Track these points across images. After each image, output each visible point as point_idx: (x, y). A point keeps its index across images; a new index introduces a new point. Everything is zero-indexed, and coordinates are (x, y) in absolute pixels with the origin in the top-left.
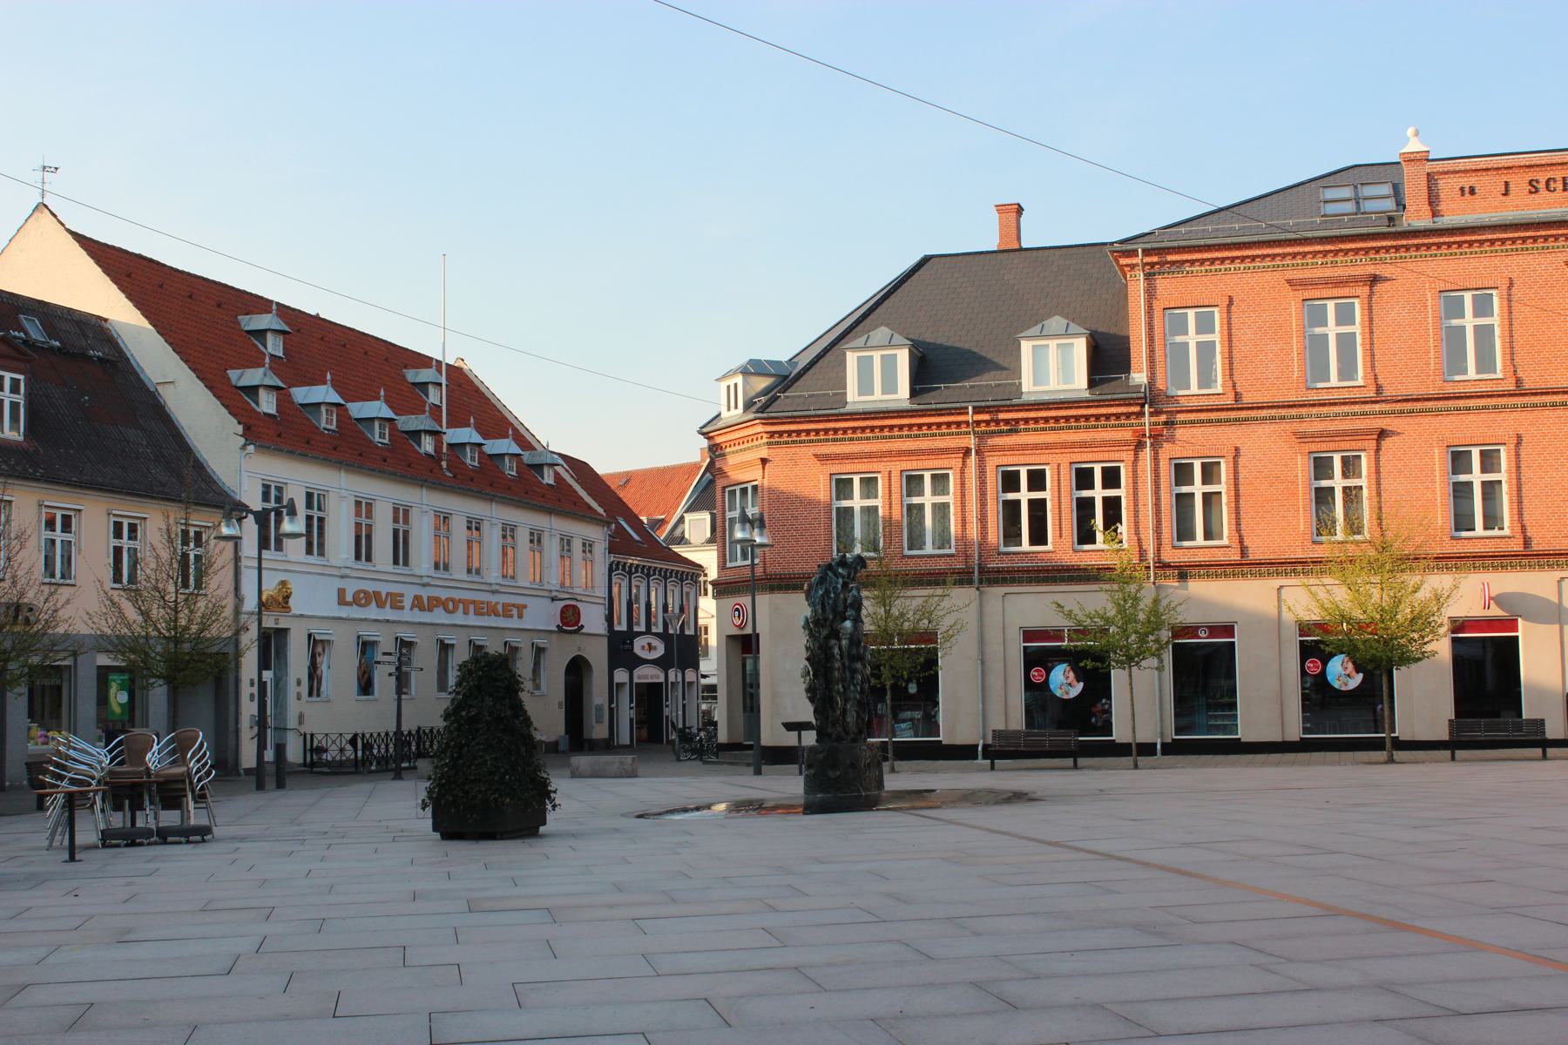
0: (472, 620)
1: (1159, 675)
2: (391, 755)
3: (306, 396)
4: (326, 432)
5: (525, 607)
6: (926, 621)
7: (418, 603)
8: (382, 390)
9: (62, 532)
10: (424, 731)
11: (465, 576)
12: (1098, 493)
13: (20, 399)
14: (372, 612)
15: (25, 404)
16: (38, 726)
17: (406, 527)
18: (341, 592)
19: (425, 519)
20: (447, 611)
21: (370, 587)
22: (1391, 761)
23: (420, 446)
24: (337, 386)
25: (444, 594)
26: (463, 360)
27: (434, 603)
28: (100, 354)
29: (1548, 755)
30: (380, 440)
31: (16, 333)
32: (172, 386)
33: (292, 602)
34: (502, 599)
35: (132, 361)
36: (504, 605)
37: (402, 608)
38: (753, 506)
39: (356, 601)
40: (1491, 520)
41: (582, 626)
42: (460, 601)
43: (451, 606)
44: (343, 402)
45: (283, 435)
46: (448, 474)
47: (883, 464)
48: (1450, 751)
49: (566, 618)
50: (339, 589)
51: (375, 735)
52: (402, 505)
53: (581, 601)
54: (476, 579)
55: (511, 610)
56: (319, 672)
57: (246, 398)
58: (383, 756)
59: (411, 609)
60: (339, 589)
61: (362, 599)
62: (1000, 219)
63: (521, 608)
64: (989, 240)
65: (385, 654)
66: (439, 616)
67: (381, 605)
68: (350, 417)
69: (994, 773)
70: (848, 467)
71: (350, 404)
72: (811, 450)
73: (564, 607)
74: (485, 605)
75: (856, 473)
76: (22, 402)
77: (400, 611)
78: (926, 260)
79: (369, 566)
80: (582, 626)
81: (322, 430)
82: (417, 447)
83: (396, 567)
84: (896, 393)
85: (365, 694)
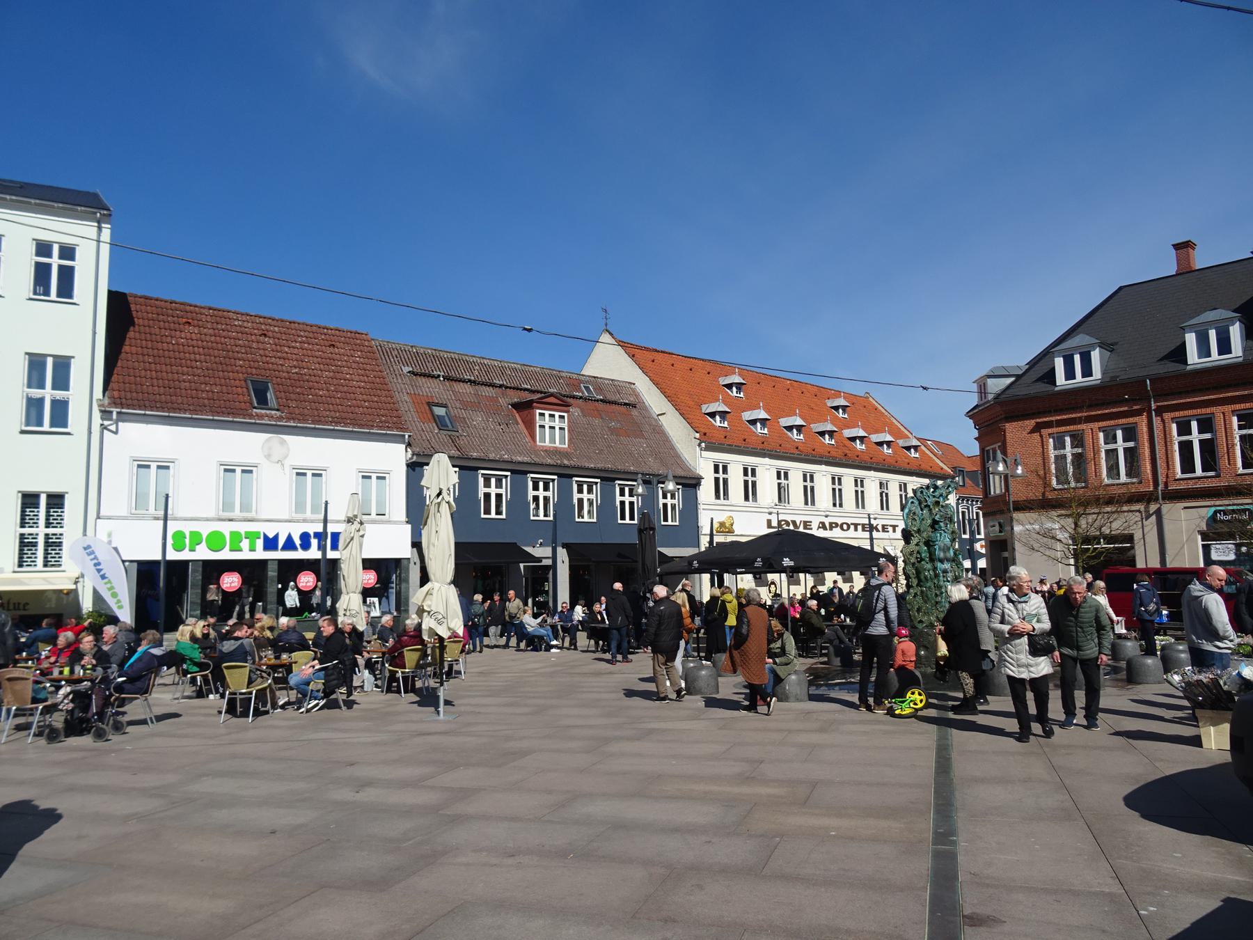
3: (749, 416)
5: (897, 526)
12: (1195, 437)
13: (565, 425)
16: (81, 643)
17: (812, 484)
20: (842, 529)
24: (767, 411)
25: (840, 521)
28: (601, 397)
40: (1133, 470)
42: (852, 524)
43: (845, 527)
62: (1177, 253)
64: (1169, 267)
68: (780, 427)
71: (872, 436)
78: (1121, 288)
79: (726, 502)
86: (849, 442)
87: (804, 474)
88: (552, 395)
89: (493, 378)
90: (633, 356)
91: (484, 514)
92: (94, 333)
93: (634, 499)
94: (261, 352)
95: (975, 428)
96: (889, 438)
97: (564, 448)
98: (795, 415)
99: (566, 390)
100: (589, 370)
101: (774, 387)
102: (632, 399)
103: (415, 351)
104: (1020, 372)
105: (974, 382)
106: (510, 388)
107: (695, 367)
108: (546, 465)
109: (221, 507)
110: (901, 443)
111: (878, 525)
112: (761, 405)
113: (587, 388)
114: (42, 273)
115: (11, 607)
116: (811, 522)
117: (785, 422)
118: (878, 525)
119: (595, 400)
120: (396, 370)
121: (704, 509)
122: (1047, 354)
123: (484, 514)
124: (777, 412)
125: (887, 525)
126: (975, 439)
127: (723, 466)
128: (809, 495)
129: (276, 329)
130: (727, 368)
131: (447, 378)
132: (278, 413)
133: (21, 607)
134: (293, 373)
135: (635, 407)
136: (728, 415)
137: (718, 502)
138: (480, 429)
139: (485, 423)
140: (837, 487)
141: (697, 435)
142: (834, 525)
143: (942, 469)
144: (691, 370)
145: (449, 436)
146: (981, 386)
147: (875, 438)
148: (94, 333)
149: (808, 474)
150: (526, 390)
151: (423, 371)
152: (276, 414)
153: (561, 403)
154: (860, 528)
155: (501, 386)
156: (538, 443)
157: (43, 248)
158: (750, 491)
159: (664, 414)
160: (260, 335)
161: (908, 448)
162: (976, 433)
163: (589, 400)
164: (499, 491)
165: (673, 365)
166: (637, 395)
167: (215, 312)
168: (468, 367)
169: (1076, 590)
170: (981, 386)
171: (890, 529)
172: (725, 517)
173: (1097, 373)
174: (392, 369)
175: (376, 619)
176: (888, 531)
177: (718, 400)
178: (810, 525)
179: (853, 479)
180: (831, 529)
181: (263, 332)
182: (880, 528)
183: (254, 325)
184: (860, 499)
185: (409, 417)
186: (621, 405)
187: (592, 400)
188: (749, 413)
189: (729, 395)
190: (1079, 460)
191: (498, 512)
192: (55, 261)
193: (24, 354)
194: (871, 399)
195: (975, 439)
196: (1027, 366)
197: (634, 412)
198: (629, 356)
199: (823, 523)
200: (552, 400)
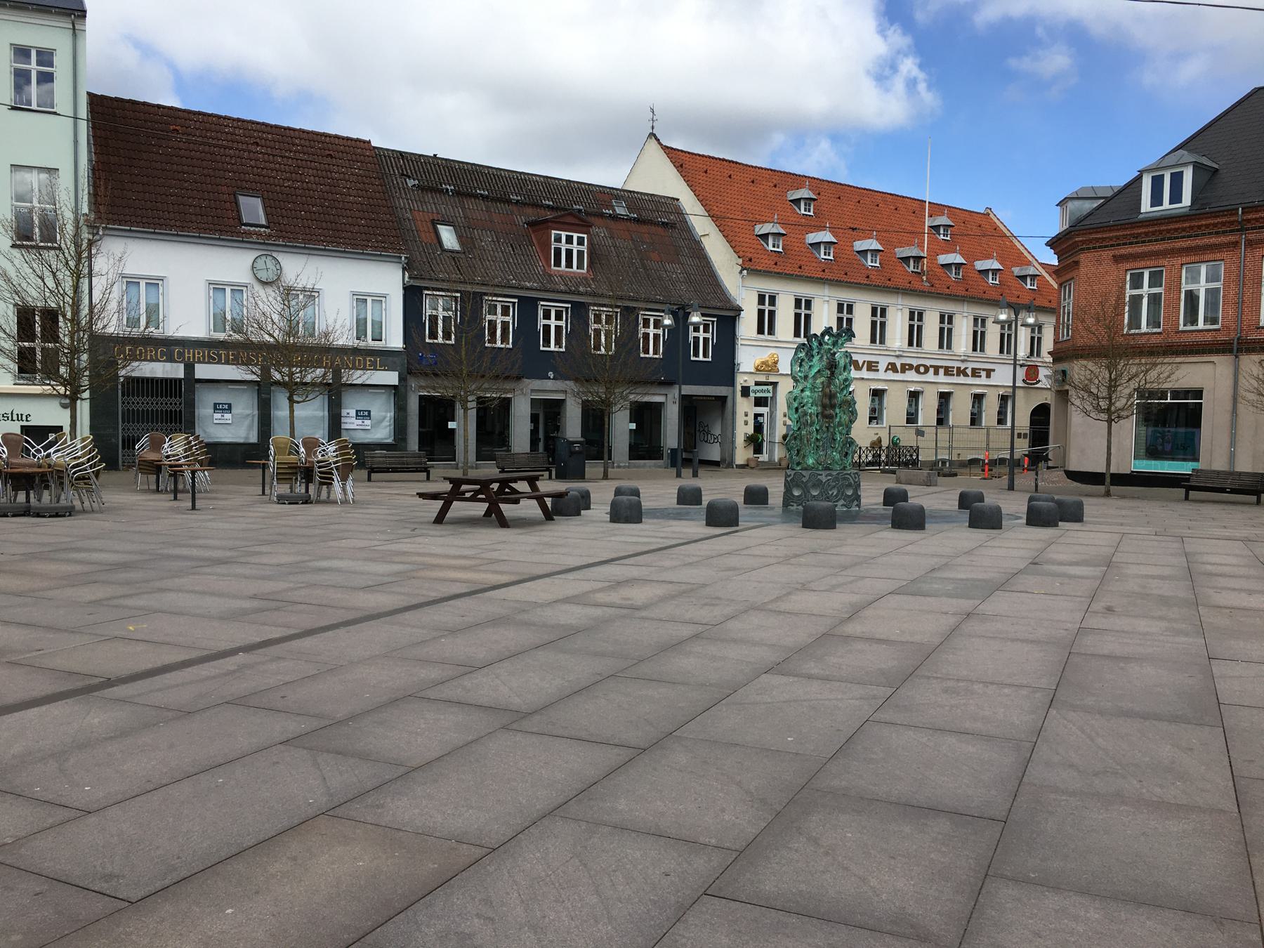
0: (942, 378)
2: (863, 462)
3: (861, 246)
5: (994, 370)
7: (892, 367)
9: (556, 320)
13: (584, 248)
20: (918, 371)
22: (1108, 494)
24: (833, 230)
25: (915, 363)
27: (905, 368)
28: (635, 215)
29: (1190, 497)
33: (779, 366)
36: (974, 370)
37: (878, 370)
42: (931, 366)
43: (922, 369)
48: (1256, 497)
51: (864, 449)
55: (980, 373)
58: (856, 462)
59: (886, 371)
69: (1187, 503)
72: (1107, 254)
74: (955, 370)
75: (1204, 262)
76: (586, 251)
77: (876, 372)
79: (770, 337)
81: (820, 259)
86: (859, 257)
91: (543, 346)
92: (76, 142)
93: (660, 332)
94: (252, 163)
97: (583, 273)
98: (955, 252)
103: (422, 161)
104: (1110, 194)
105: (1057, 205)
106: (529, 205)
109: (212, 327)
114: (21, 78)
115: (15, 417)
116: (878, 363)
120: (400, 184)
121: (741, 345)
123: (543, 346)
124: (971, 257)
125: (980, 369)
127: (948, 316)
129: (270, 136)
131: (457, 193)
132: (268, 231)
133: (24, 418)
134: (286, 187)
137: (761, 336)
138: (489, 251)
139: (495, 245)
140: (979, 329)
141: (740, 261)
142: (907, 367)
144: (753, 182)
145: (454, 258)
148: (76, 142)
151: (499, 196)
152: (265, 232)
153: (579, 222)
154: (941, 371)
156: (552, 267)
157: (22, 52)
159: (708, 235)
160: (252, 144)
164: (559, 323)
165: (730, 177)
167: (205, 118)
168: (482, 180)
169: (934, 459)
171: (983, 374)
172: (767, 356)
173: (1187, 199)
174: (395, 182)
175: (372, 446)
176: (980, 376)
178: (877, 366)
180: (903, 371)
181: (329, 153)
182: (969, 372)
183: (246, 132)
184: (945, 338)
185: (410, 237)
188: (860, 242)
191: (705, 356)
192: (33, 66)
193: (9, 166)
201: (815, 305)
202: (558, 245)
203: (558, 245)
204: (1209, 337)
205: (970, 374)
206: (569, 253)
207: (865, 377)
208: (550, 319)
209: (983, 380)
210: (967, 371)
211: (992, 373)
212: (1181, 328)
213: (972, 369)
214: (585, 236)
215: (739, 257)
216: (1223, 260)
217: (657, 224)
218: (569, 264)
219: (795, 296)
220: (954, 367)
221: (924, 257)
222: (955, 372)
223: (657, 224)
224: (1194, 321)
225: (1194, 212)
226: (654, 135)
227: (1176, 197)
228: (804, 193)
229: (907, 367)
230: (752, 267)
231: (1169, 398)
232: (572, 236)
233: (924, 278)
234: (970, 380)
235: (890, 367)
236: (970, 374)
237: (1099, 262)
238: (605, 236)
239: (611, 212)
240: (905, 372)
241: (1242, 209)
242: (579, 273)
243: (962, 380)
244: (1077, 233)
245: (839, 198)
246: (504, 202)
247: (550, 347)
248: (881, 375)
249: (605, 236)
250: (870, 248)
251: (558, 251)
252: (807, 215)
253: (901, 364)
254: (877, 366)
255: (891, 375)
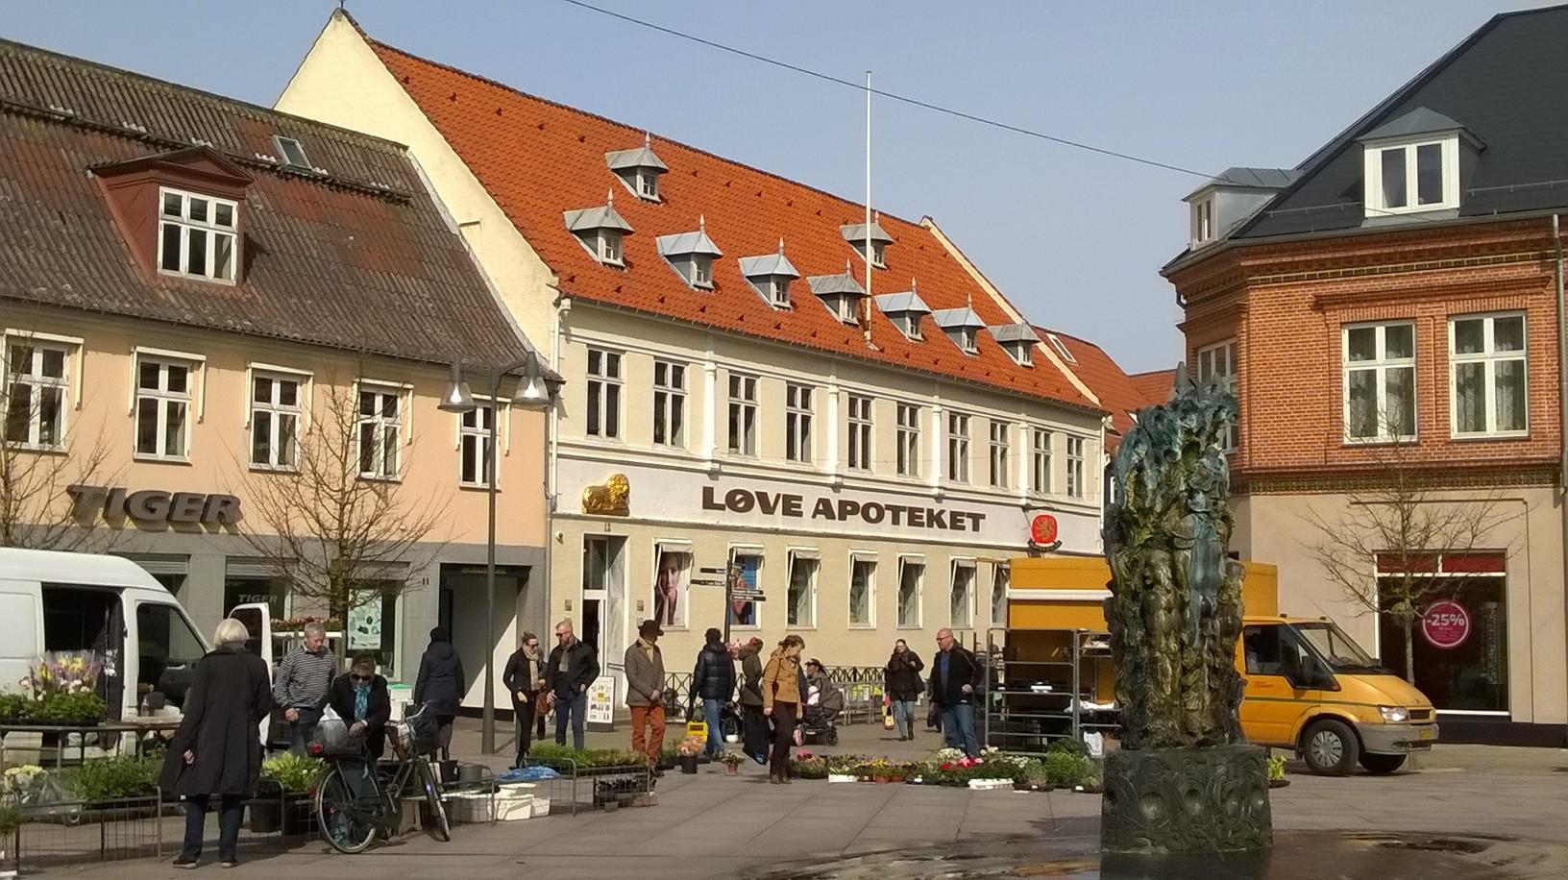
0: (904, 531)
1: (169, 848)
4: (697, 290)
5: (983, 517)
6: (1469, 535)
7: (824, 508)
8: (611, 192)
10: (844, 672)
11: (583, 439)
14: (755, 518)
15: (238, 240)
18: (708, 493)
19: (936, 419)
20: (867, 517)
21: (752, 487)
23: (837, 312)
25: (862, 498)
26: (931, 219)
27: (847, 509)
28: (325, 172)
30: (778, 303)
31: (265, 157)
32: (478, 226)
34: (949, 507)
35: (434, 198)
36: (953, 515)
37: (800, 514)
38: (1232, 373)
39: (731, 501)
41: (1060, 543)
42: (888, 507)
43: (873, 514)
44: (928, 309)
45: (818, 335)
46: (872, 347)
47: (1419, 306)
49: (1040, 532)
50: (704, 488)
51: (861, 672)
52: (745, 374)
53: (1058, 511)
54: (909, 480)
55: (962, 521)
56: (671, 593)
57: (582, 244)
59: (814, 516)
60: (704, 488)
61: (739, 501)
63: (976, 518)
65: (703, 570)
66: (855, 525)
67: (768, 509)
68: (740, 275)
70: (1371, 313)
72: (1307, 293)
73: (1037, 518)
74: (925, 515)
78: (1498, 20)
79: (610, 443)
80: (1060, 543)
82: (834, 314)
83: (790, 461)
84: (1441, 201)
85: (742, 623)
87: (850, 399)
88: (203, 153)
89: (48, 100)
90: (405, 82)
95: (1179, 301)
96: (974, 320)
97: (227, 288)
99: (234, 146)
100: (296, 103)
101: (728, 185)
102: (399, 184)
104: (1285, 184)
105: (1184, 200)
106: (94, 128)
107: (552, 122)
108: (180, 324)
110: (997, 332)
111: (942, 512)
112: (702, 221)
113: (289, 146)
116: (800, 498)
117: (750, 265)
118: (942, 512)
119: (307, 178)
121: (559, 456)
122: (1344, 152)
125: (962, 514)
126: (1178, 326)
128: (797, 431)
130: (632, 137)
135: (407, 203)
136: (626, 240)
142: (849, 508)
143: (1080, 395)
144: (541, 127)
146: (1200, 207)
147: (944, 317)
149: (743, 379)
150: (137, 136)
154: (904, 516)
155: (68, 121)
156: (160, 269)
158: (667, 417)
159: (477, 223)
161: (1011, 344)
162: (1181, 315)
163: (293, 174)
165: (499, 112)
166: (409, 173)
170: (1200, 207)
171: (968, 522)
173: (1451, 197)
176: (963, 528)
177: (604, 203)
179: (1066, 437)
180: (842, 517)
182: (946, 518)
186: (373, 195)
187: (300, 177)
189: (628, 194)
190: (1403, 387)
194: (934, 231)
195: (1178, 326)
196: (1301, 173)
197: (409, 215)
198: (397, 78)
199: (825, 502)
200: (205, 167)
201: (688, 373)
202: (172, 220)
203: (172, 220)
204: (1509, 454)
205: (948, 523)
206: (198, 239)
207: (782, 527)
208: (156, 387)
209: (966, 536)
210: (943, 516)
211: (981, 521)
212: (1455, 435)
213: (952, 513)
214: (234, 204)
215: (553, 271)
216: (1526, 309)
217: (369, 193)
218: (198, 265)
219: (655, 357)
220: (922, 510)
221: (866, 296)
222: (925, 520)
223: (369, 193)
224: (1370, 429)
225: (1469, 220)
226: (344, 12)
227: (1430, 189)
228: (642, 157)
229: (849, 508)
230: (579, 294)
231: (1440, 568)
232: (206, 202)
233: (868, 334)
234: (948, 535)
235: (821, 507)
236: (948, 525)
237: (1287, 307)
238: (266, 208)
239: (273, 159)
240: (845, 519)
241: (1559, 217)
242: (190, 282)
243: (934, 534)
244: (1244, 250)
245: (695, 174)
246: (37, 119)
247: (154, 451)
248: (806, 523)
249: (266, 208)
250: (776, 272)
251: (172, 234)
252: (648, 200)
253: (840, 502)
254: (799, 506)
255: (823, 525)
